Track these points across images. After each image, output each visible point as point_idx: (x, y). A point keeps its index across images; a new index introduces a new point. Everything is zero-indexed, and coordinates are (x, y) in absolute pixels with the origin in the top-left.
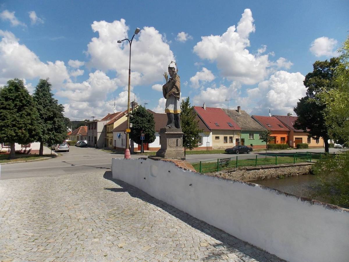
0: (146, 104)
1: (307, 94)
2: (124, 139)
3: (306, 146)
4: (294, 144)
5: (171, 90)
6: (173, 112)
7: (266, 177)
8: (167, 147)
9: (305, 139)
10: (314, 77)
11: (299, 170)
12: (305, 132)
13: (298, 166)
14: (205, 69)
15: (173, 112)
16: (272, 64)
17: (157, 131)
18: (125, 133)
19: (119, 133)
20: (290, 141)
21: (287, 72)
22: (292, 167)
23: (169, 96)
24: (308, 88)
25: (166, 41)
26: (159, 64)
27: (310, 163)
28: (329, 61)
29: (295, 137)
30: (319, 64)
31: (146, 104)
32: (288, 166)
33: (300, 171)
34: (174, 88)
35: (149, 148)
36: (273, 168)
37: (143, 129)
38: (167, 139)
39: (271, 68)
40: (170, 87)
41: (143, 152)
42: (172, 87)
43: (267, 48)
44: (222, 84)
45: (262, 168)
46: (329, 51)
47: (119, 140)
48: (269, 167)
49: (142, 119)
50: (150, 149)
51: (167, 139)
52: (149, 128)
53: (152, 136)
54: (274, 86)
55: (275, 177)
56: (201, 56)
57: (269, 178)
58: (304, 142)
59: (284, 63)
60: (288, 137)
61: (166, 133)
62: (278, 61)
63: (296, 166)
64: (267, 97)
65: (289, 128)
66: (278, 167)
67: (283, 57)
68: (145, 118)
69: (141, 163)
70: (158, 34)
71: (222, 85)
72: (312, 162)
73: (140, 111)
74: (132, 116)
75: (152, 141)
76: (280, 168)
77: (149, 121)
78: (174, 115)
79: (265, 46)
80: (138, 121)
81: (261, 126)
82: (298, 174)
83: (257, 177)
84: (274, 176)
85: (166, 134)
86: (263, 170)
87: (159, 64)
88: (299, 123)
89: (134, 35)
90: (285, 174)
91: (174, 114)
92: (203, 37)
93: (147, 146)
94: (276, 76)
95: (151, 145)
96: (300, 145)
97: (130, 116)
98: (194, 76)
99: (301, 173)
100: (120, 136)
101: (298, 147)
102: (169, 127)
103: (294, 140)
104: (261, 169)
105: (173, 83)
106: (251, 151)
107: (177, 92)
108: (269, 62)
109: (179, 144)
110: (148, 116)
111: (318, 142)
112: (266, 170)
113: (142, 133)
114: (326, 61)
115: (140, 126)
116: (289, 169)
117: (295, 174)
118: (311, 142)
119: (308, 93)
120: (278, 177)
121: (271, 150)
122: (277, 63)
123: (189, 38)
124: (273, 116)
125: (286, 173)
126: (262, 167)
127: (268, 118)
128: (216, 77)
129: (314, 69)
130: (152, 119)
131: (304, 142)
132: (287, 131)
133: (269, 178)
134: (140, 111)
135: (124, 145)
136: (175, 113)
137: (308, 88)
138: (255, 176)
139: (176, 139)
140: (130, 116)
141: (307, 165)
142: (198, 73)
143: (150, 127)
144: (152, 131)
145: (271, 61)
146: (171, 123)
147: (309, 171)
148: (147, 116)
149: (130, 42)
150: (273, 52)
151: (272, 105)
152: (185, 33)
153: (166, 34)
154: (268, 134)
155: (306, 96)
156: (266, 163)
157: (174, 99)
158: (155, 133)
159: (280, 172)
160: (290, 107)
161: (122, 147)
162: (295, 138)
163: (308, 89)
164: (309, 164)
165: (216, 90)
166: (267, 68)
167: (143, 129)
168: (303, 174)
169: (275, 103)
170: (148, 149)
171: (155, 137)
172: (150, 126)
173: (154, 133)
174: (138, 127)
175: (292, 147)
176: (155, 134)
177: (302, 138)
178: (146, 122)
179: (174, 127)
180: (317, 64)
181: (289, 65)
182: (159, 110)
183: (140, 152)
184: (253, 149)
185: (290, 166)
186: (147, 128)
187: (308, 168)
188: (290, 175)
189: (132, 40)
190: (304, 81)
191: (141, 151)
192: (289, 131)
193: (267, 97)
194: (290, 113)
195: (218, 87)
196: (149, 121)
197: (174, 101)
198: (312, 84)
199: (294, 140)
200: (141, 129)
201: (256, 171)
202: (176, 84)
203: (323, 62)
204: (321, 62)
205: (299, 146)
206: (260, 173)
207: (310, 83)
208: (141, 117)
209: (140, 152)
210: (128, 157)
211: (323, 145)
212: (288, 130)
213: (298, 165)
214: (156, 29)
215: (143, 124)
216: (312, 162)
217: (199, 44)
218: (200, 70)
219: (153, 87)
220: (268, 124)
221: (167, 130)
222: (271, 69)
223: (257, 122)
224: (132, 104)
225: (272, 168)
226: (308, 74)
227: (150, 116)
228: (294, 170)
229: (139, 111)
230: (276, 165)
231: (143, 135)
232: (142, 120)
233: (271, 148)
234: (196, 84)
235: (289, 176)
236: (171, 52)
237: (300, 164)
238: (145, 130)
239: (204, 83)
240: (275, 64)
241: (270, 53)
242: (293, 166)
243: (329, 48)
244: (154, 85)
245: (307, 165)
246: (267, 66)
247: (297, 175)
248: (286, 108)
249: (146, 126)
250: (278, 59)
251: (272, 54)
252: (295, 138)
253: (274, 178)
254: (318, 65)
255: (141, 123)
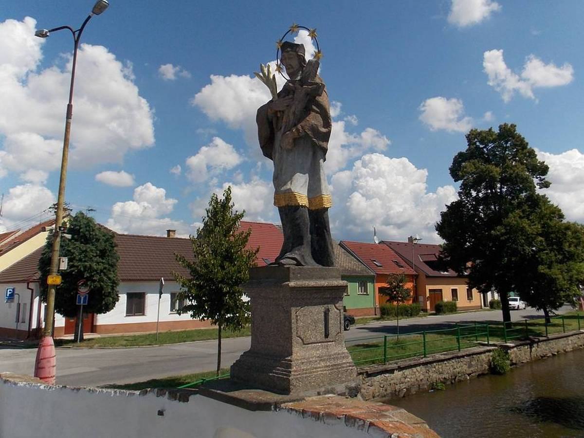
0: (92, 210)
1: (460, 196)
2: (25, 304)
3: (452, 308)
4: (428, 303)
5: (300, 120)
6: (307, 205)
7: (408, 390)
8: (294, 343)
9: (447, 291)
10: (472, 161)
11: (470, 366)
12: (461, 276)
13: (468, 355)
14: (219, 141)
15: (307, 205)
16: (352, 139)
17: (123, 280)
18: (28, 288)
19: (9, 288)
20: (420, 297)
21: (383, 155)
22: (457, 360)
23: (295, 140)
24: (460, 182)
25: (133, 77)
26: (114, 125)
27: (488, 348)
28: (496, 130)
29: (429, 287)
30: (477, 134)
31: (92, 210)
32: (449, 359)
33: (472, 369)
34: (313, 114)
35: (96, 326)
36: (421, 366)
37: (86, 275)
38: (293, 310)
39: (350, 147)
40: (297, 107)
41: (82, 340)
42: (307, 110)
43: (341, 108)
44: (256, 174)
45: (400, 369)
46: (450, 121)
47: (10, 307)
48: (412, 363)
49: (83, 247)
50: (98, 329)
51: (293, 310)
52: (102, 271)
53: (109, 293)
54: (362, 182)
55: (426, 387)
56: (210, 113)
57: (413, 391)
58: (445, 300)
59: (376, 139)
60: (416, 288)
61: (292, 284)
62: (363, 134)
63: (463, 357)
64: (348, 204)
65: (417, 269)
66: (431, 363)
67: (372, 128)
68: (93, 245)
69: (161, 413)
70: (114, 61)
71: (256, 178)
72: (491, 345)
73: (80, 226)
74: (69, 236)
75: (107, 308)
76: (435, 364)
77: (103, 254)
78: (309, 212)
79: (339, 104)
80: (73, 253)
81: (360, 263)
82: (469, 375)
83: (389, 391)
84: (423, 384)
85: (294, 288)
86: (401, 373)
87: (114, 125)
88: (446, 257)
89: (89, 17)
90: (445, 378)
91: (309, 210)
92: (216, 77)
93: (90, 321)
94: (365, 165)
95: (102, 319)
96: (441, 306)
97: (62, 237)
98: (194, 155)
99: (475, 372)
100: (12, 296)
101: (439, 309)
102: (295, 262)
103: (428, 295)
104: (396, 369)
105: (307, 94)
106: (351, 324)
107: (324, 130)
108: (347, 137)
109: (333, 330)
110: (101, 240)
111: (470, 298)
112: (407, 372)
113: (82, 284)
114: (490, 130)
115: (77, 267)
116: (452, 366)
117: (463, 377)
118: (459, 299)
119: (461, 193)
120: (433, 386)
121: (388, 319)
122: (361, 138)
123: (181, 74)
124: (381, 242)
125: (446, 376)
126: (399, 364)
127: (373, 247)
128: (242, 159)
129: (468, 145)
130: (113, 247)
131: (445, 300)
132: (412, 276)
133: (415, 392)
134: (80, 226)
135: (24, 322)
136: (311, 209)
137: (460, 182)
138: (386, 390)
139: (321, 309)
140: (62, 237)
141: (484, 352)
142: (204, 149)
143: (105, 268)
144: (110, 279)
145: (351, 133)
146: (302, 244)
147: (488, 365)
148: (98, 240)
149: (76, 36)
150: (355, 116)
151: (358, 221)
152: (174, 66)
153: (132, 63)
154: (401, 281)
155: (459, 199)
156: (401, 353)
157: (311, 153)
158: (117, 284)
159: (435, 375)
160: (392, 226)
161: (15, 328)
162: (430, 290)
163: (462, 184)
164: (489, 351)
165: (245, 187)
166: (343, 146)
167: (86, 275)
168: (479, 376)
169: (363, 217)
170: (93, 329)
171: (117, 295)
172: (107, 266)
173: (114, 284)
174: (72, 269)
175: (425, 310)
176: (118, 288)
177: (441, 290)
178: (96, 256)
179: (311, 264)
180: (473, 134)
181: (383, 142)
182: (117, 227)
183: (73, 338)
184: (355, 318)
185: (452, 358)
186: (98, 273)
187: (486, 360)
188: (455, 379)
189: (81, 30)
190: (450, 169)
191: (76, 336)
192: (415, 275)
193: (348, 204)
194: (414, 237)
195: (248, 180)
196: (103, 254)
197: (309, 164)
198: (468, 173)
199: (428, 295)
200: (80, 274)
201: (387, 375)
202: (318, 98)
203: (485, 132)
204: (481, 132)
205: (441, 308)
206: (395, 381)
207: (465, 172)
208: (82, 243)
209: (73, 338)
210: (49, 362)
211: (480, 305)
212: (415, 273)
213: (468, 353)
214: (111, 51)
215: (85, 261)
216: (491, 345)
217: (206, 90)
218: (208, 142)
219: (99, 176)
220: (375, 261)
221: (291, 272)
222: (350, 149)
223: (353, 255)
224: (56, 208)
225: (419, 365)
226: (458, 154)
227: (107, 240)
228: (461, 367)
229: (76, 225)
230: (425, 357)
231: (84, 290)
232: (83, 252)
233: (388, 314)
234: (200, 172)
235: (453, 381)
236: (144, 101)
237: (471, 352)
238: (90, 279)
239: (218, 171)
240: (357, 140)
241: (349, 118)
242: (458, 357)
243: (451, 117)
244: (101, 172)
245: (484, 352)
246: (343, 143)
247: (468, 378)
248: (384, 228)
249: (95, 267)
250: (364, 129)
251: (353, 121)
252: (430, 290)
253: (426, 391)
254: (475, 137)
255: (80, 260)
